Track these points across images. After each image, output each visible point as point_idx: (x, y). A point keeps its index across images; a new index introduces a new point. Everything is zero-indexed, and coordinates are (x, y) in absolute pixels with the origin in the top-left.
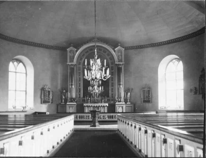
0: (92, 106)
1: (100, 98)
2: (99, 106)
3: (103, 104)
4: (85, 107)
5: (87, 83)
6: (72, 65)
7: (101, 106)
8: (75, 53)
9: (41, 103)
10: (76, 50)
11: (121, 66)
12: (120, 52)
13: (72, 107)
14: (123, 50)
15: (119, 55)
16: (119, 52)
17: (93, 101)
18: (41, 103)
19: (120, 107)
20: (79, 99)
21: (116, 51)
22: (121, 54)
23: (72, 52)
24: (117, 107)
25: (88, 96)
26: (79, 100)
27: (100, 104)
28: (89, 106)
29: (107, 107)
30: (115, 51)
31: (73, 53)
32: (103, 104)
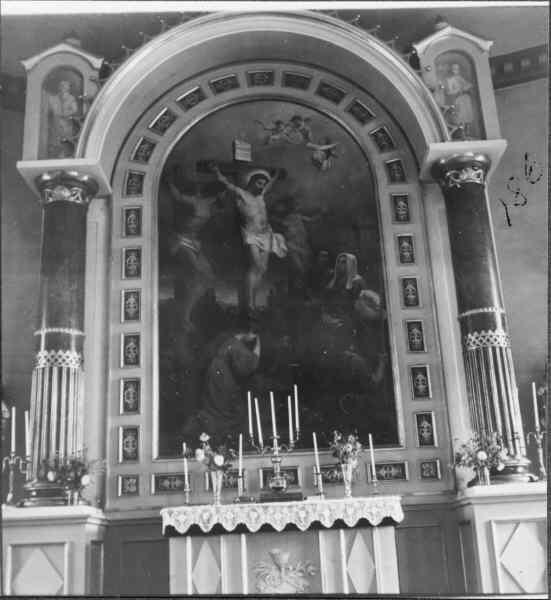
0: (241, 529)
1: (316, 452)
2: (317, 526)
3: (350, 500)
4: (173, 542)
5: (474, 342)
6: (63, 179)
7: (339, 524)
8: (89, 89)
9: (123, 197)
10: (98, 63)
11: (471, 175)
12: (456, 67)
13: (42, 545)
14: (481, 50)
15: (452, 92)
16: (450, 73)
17: (253, 487)
18: (123, 197)
19: (517, 523)
20: (130, 469)
21: (423, 63)
22: (468, 86)
23: (65, 85)
24: (489, 525)
25: (205, 438)
26: (126, 478)
27: (321, 508)
28: (218, 530)
29: (391, 530)
30: (414, 62)
31: (77, 91)
32: (349, 506)
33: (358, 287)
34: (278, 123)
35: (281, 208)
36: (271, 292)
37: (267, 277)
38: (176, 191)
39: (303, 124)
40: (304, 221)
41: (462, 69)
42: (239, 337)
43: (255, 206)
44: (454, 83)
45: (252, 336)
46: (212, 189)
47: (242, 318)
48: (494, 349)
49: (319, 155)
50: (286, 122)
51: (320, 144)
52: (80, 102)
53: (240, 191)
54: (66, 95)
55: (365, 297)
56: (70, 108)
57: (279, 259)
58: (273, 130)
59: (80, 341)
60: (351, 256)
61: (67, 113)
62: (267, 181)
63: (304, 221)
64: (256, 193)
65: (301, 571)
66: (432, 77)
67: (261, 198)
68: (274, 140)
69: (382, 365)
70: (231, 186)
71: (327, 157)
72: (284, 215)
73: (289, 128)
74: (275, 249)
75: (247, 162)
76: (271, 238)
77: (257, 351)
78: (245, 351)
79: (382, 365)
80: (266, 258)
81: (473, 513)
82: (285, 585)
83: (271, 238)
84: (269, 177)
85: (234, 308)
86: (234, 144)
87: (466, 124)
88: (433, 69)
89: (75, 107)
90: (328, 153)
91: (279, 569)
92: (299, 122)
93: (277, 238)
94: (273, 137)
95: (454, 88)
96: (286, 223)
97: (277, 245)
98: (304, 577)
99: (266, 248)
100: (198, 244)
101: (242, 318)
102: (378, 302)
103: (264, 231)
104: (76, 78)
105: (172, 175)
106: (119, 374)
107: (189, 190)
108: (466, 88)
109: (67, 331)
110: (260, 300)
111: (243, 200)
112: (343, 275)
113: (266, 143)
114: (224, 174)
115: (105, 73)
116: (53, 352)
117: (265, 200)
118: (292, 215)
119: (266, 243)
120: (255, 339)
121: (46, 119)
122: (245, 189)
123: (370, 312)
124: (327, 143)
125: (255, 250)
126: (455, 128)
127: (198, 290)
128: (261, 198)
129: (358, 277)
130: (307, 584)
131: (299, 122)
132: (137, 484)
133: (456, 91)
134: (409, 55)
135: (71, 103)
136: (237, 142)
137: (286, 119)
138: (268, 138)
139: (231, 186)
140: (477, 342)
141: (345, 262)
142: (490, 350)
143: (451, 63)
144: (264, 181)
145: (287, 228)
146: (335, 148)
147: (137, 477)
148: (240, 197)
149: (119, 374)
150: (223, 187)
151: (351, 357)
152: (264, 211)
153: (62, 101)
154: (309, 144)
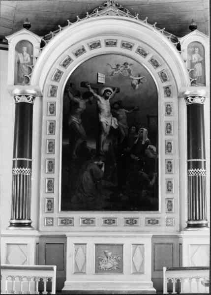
8: (36, 51)
16: (194, 52)
21: (182, 47)
30: (179, 48)
33: (147, 144)
34: (118, 65)
35: (116, 106)
36: (110, 144)
37: (109, 137)
38: (71, 96)
39: (129, 66)
40: (126, 112)
41: (199, 51)
42: (96, 163)
43: (105, 105)
44: (196, 57)
45: (101, 162)
46: (87, 95)
47: (97, 154)
48: (199, 176)
49: (135, 82)
50: (122, 65)
51: (136, 77)
52: (32, 58)
53: (99, 97)
54: (25, 53)
55: (150, 148)
56: (27, 60)
57: (114, 129)
58: (115, 68)
59: (30, 163)
60: (145, 130)
61: (26, 62)
62: (111, 93)
63: (126, 112)
64: (106, 98)
65: (115, 259)
66: (185, 54)
67: (108, 100)
68: (116, 74)
69: (154, 178)
70: (95, 95)
71: (139, 83)
72: (117, 109)
73: (122, 68)
74: (113, 125)
75: (103, 83)
76: (111, 120)
77: (103, 169)
78: (98, 169)
79: (154, 178)
80: (108, 127)
81: (182, 241)
82: (109, 264)
83: (111, 120)
84: (112, 91)
85: (94, 150)
86: (97, 74)
87: (198, 77)
88: (186, 51)
89: (29, 59)
90: (139, 81)
91: (108, 258)
92: (127, 66)
93: (114, 121)
94: (115, 72)
95: (195, 59)
96: (118, 113)
97: (114, 123)
98: (116, 261)
99: (109, 124)
100: (80, 120)
101: (97, 154)
102: (155, 151)
103: (108, 116)
104: (30, 45)
105: (70, 85)
106: (102, 40)
107: (78, 95)
108: (200, 60)
109: (26, 159)
110: (105, 147)
111: (100, 101)
112: (141, 138)
113: (112, 75)
114: (92, 88)
115: (43, 45)
116: (21, 168)
117: (110, 102)
118: (121, 110)
119: (109, 121)
120: (102, 164)
121: (17, 64)
122: (101, 96)
123: (152, 155)
124: (139, 76)
125: (104, 125)
126: (193, 80)
127: (80, 141)
128: (108, 100)
129: (147, 139)
130: (117, 263)
131: (127, 66)
132: (53, 222)
133: (196, 61)
134: (177, 43)
135: (27, 56)
136: (99, 74)
137: (121, 64)
138: (113, 73)
139: (95, 95)
140: (193, 173)
141: (142, 132)
142: (197, 177)
143: (194, 47)
144: (110, 93)
145: (119, 115)
146: (142, 79)
147: (52, 218)
148: (99, 100)
149: (102, 40)
150: (92, 94)
151: (142, 174)
152: (109, 107)
153: (24, 56)
154: (131, 77)
